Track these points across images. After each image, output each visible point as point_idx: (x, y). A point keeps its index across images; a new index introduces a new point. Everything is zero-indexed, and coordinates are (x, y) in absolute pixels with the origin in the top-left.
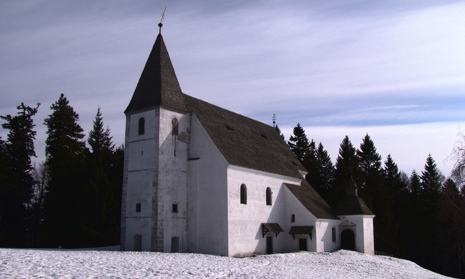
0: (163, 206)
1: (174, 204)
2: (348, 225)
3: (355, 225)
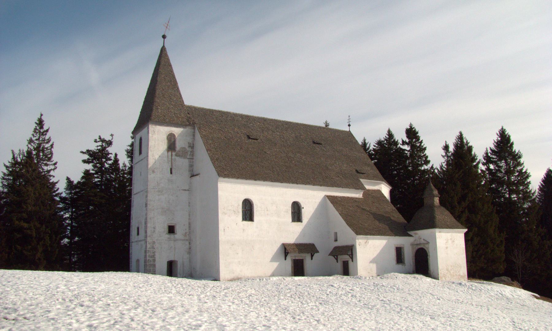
0: (154, 228)
1: (170, 225)
2: (421, 243)
3: (428, 243)
